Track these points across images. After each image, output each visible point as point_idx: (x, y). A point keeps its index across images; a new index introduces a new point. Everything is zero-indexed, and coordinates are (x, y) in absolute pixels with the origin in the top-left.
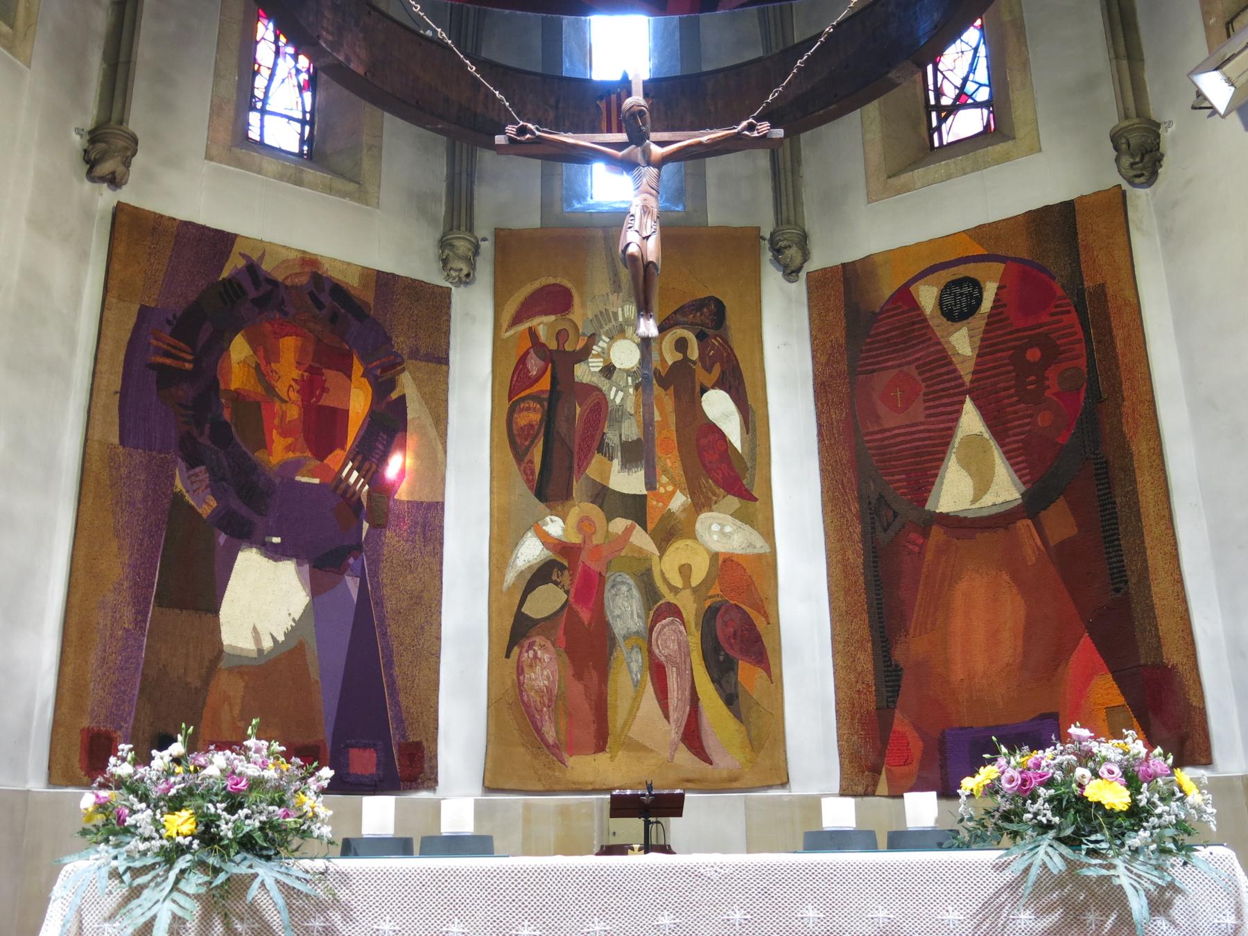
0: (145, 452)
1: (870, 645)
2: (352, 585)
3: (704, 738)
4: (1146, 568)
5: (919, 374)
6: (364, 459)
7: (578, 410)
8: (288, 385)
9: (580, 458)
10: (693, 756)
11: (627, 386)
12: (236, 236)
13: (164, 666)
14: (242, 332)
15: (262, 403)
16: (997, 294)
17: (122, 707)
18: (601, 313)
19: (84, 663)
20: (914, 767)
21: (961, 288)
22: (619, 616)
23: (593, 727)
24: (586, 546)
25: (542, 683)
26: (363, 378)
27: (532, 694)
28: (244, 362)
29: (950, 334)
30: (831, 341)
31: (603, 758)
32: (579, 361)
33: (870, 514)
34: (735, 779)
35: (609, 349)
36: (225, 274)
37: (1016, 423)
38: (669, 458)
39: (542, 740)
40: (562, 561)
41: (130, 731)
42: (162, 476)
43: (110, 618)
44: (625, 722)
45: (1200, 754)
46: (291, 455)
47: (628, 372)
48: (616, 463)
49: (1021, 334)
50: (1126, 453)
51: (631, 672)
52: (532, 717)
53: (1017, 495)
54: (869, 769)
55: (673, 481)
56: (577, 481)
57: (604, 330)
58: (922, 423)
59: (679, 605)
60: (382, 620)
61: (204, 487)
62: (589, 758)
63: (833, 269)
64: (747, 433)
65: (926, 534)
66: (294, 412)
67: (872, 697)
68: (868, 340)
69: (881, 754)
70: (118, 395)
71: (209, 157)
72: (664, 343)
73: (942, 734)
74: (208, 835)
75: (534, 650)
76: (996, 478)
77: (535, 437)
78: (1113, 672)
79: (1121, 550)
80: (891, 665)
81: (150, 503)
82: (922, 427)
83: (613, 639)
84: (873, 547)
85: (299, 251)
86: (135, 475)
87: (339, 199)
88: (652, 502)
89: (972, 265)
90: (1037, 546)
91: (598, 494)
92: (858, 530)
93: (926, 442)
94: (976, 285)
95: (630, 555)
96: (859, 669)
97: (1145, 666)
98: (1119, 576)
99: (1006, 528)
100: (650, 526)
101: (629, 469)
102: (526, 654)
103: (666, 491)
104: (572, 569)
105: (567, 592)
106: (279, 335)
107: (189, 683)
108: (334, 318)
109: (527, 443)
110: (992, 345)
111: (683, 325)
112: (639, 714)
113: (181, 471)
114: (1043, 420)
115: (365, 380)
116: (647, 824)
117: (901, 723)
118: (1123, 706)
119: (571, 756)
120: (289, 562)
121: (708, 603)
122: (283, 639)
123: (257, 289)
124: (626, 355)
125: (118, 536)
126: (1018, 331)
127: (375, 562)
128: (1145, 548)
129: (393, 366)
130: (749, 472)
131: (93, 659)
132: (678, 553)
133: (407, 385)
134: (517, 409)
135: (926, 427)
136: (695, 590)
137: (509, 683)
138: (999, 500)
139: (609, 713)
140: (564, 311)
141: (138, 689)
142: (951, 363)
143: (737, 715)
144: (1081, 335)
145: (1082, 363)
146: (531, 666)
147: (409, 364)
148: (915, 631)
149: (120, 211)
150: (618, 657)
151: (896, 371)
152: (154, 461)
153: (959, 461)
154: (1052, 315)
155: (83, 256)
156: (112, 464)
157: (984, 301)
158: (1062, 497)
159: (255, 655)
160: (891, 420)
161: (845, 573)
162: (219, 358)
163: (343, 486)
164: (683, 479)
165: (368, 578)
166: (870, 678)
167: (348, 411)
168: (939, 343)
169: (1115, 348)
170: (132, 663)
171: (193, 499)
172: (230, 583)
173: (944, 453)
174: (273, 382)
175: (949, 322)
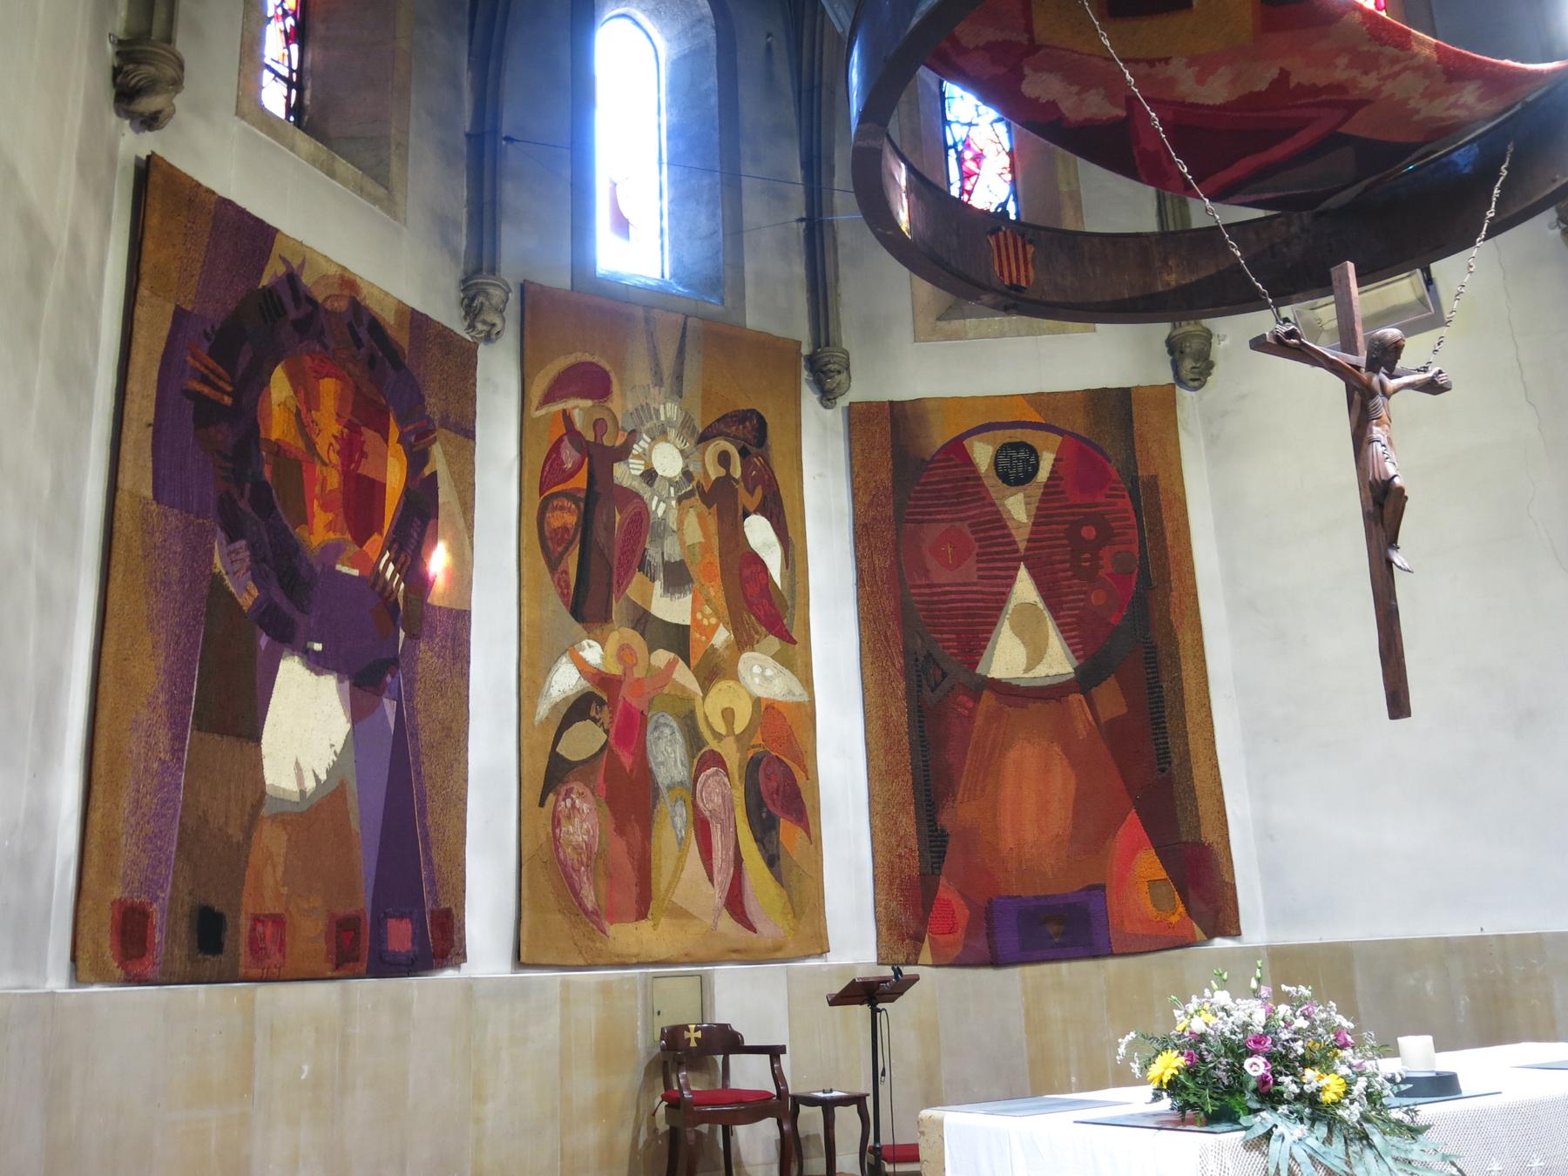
0: (181, 514)
1: (912, 807)
3: (746, 903)
4: (1188, 752)
5: (973, 533)
6: (401, 549)
7: (618, 518)
8: (328, 442)
9: (619, 574)
10: (736, 923)
11: (669, 497)
12: (277, 230)
13: (204, 812)
14: (283, 363)
15: (303, 463)
16: (1053, 466)
17: (158, 871)
18: (642, 407)
19: (114, 807)
20: (960, 934)
21: (1018, 453)
22: (662, 763)
23: (635, 890)
24: (627, 679)
25: (580, 838)
26: (398, 445)
27: (569, 850)
28: (283, 404)
29: (1005, 497)
30: (876, 482)
31: (645, 925)
32: (619, 459)
33: (917, 671)
35: (651, 450)
36: (265, 281)
37: (1071, 597)
38: (713, 586)
39: (580, 904)
40: (601, 695)
41: (167, 902)
42: (198, 554)
43: (143, 744)
44: (669, 884)
45: (1230, 926)
46: (332, 536)
47: (671, 482)
48: (658, 585)
49: (1076, 510)
50: (1172, 641)
51: (675, 827)
52: (569, 877)
53: (1070, 669)
54: (910, 937)
55: (716, 612)
56: (617, 602)
57: (645, 427)
58: (975, 584)
59: (722, 754)
60: (417, 754)
61: (245, 569)
62: (631, 926)
63: (880, 405)
64: (787, 568)
65: (976, 699)
66: (334, 480)
67: (916, 863)
68: (917, 488)
69: (923, 921)
70: (151, 428)
72: (707, 453)
73: (989, 903)
75: (572, 799)
76: (1049, 650)
77: (571, 543)
78: (1156, 848)
79: (1166, 733)
80: (937, 830)
81: (187, 586)
82: (975, 588)
83: (657, 789)
84: (919, 706)
85: (340, 266)
86: (171, 544)
87: (365, 202)
88: (695, 635)
89: (1029, 431)
90: (1088, 720)
91: (639, 620)
92: (903, 685)
93: (979, 604)
95: (673, 693)
96: (902, 833)
97: (1185, 843)
98: (1164, 755)
99: (1059, 701)
100: (694, 662)
101: (672, 594)
102: (563, 803)
103: (709, 623)
104: (612, 702)
105: (607, 732)
106: (322, 375)
107: (231, 836)
109: (560, 549)
110: (1046, 516)
111: (727, 436)
112: (684, 875)
113: (220, 544)
114: (1097, 599)
115: (400, 447)
116: (875, 1011)
117: (947, 891)
118: (1165, 880)
119: (612, 924)
120: (331, 677)
122: (325, 778)
123: (297, 308)
124: (668, 460)
125: (152, 629)
126: (1075, 506)
128: (1187, 733)
130: (789, 611)
131: (125, 804)
134: (550, 506)
135: (979, 588)
136: (738, 738)
137: (543, 837)
138: (1052, 672)
139: (653, 875)
140: (601, 397)
141: (175, 844)
142: (1005, 527)
143: (778, 877)
144: (1134, 521)
146: (569, 818)
147: (441, 433)
148: (963, 796)
150: (661, 811)
151: (949, 525)
152: (191, 528)
153: (1012, 628)
154: (1108, 496)
156: (145, 526)
157: (1040, 469)
158: (1113, 675)
159: (296, 798)
160: (942, 576)
161: (886, 730)
162: (259, 395)
163: (381, 582)
164: (726, 612)
165: (404, 702)
166: (913, 843)
167: (384, 486)
168: (993, 504)
169: (1165, 540)
170: (168, 809)
171: (233, 584)
172: (272, 701)
173: (997, 617)
174: (314, 436)
175: (1005, 485)
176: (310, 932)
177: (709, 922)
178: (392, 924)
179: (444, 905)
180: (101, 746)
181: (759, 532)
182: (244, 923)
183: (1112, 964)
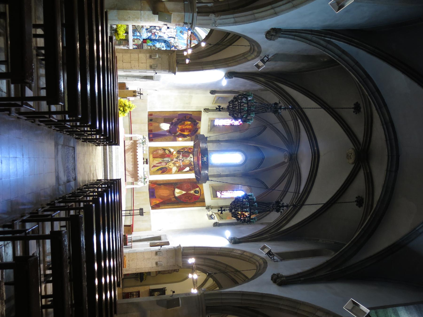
20: (152, 186)
23: (155, 157)
34: (150, 170)
36: (197, 121)
65: (173, 188)
66: (184, 128)
69: (153, 184)
71: (209, 118)
74: (144, 142)
83: (164, 159)
94: (198, 193)
98: (168, 204)
100: (175, 162)
104: (170, 154)
106: (191, 126)
108: (194, 131)
117: (155, 185)
127: (170, 136)
129: (190, 136)
132: (172, 165)
133: (188, 138)
136: (168, 166)
143: (156, 171)
145: (188, 202)
147: (191, 138)
149: (201, 111)
166: (160, 183)
167: (185, 132)
176: (151, 128)
177: (153, 164)
179: (153, 140)
180: (162, 112)
181: (187, 169)
182: (152, 123)
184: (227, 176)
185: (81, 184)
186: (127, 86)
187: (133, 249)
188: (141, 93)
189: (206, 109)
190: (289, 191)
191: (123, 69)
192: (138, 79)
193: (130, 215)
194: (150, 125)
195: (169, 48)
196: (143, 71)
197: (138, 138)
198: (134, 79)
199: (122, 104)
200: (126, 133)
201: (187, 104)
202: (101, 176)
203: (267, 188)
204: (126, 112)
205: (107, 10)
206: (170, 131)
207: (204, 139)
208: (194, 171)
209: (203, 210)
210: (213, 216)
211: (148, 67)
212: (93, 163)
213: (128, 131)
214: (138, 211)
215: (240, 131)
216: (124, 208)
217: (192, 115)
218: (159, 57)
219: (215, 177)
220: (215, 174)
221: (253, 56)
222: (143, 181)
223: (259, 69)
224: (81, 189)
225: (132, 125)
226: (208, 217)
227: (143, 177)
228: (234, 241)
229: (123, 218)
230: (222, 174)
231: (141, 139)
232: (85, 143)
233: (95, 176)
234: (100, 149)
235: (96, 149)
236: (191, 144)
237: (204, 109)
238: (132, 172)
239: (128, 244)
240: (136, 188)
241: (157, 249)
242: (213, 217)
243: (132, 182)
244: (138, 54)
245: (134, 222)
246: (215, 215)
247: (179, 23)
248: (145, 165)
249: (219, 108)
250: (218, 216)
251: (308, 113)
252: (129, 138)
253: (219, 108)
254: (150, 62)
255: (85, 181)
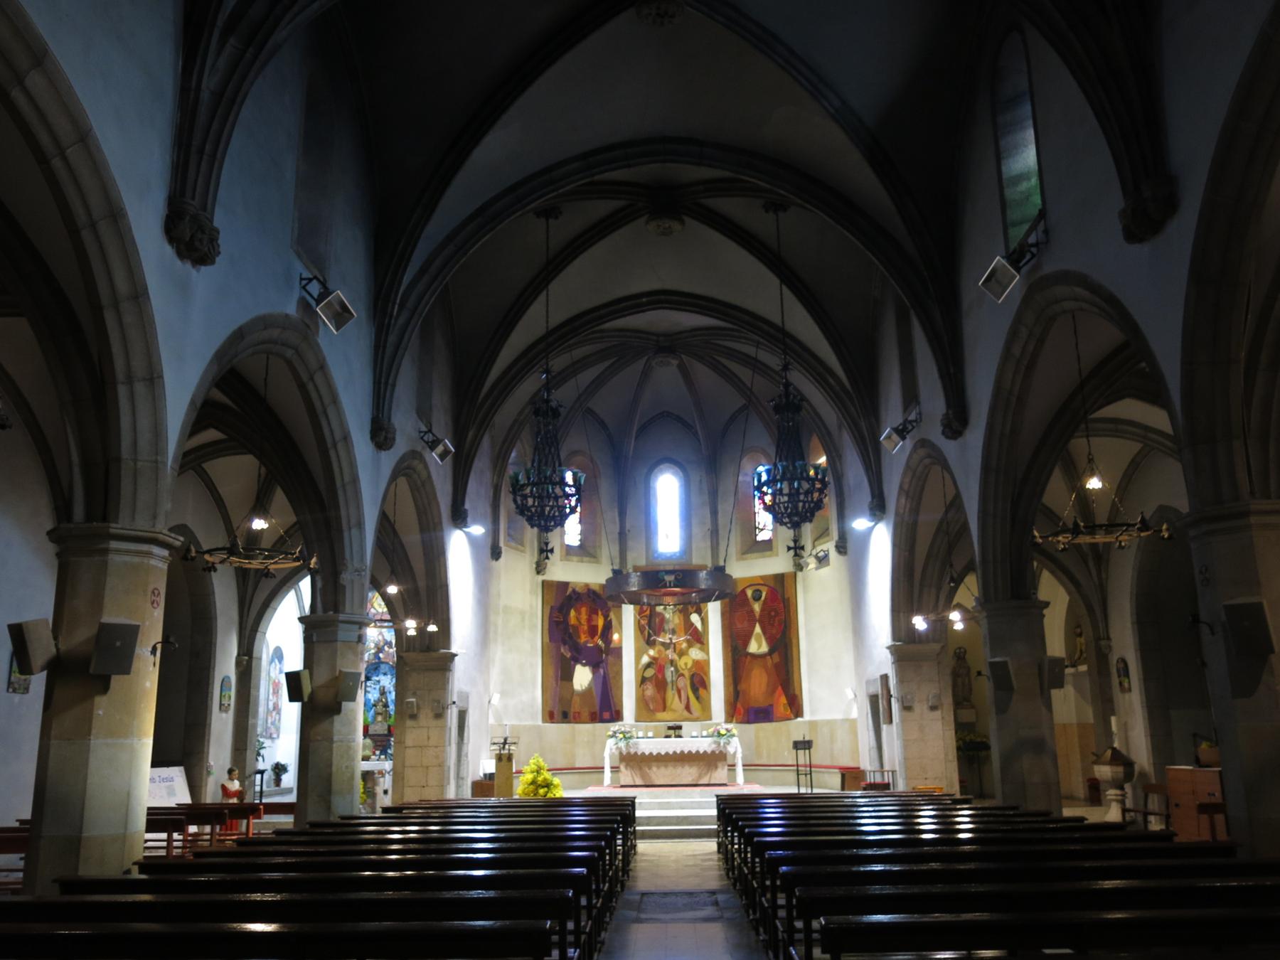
2: (601, 671)
36: (568, 593)
42: (559, 649)
50: (791, 640)
65: (746, 657)
66: (586, 628)
71: (561, 560)
74: (624, 737)
94: (761, 592)
100: (677, 652)
104: (657, 663)
108: (594, 600)
117: (739, 705)
121: (691, 673)
127: (607, 664)
132: (684, 659)
133: (612, 616)
145: (783, 617)
147: (612, 609)
149: (544, 582)
155: (537, 595)
160: (739, 626)
176: (585, 714)
178: (604, 713)
179: (617, 709)
181: (695, 618)
182: (572, 714)
183: (774, 724)
184: (714, 513)
185: (726, 882)
186: (480, 777)
187: (897, 769)
188: (502, 741)
189: (536, 568)
190: (754, 356)
191: (443, 786)
192: (465, 748)
193: (811, 774)
194: (577, 719)
195: (379, 666)
196: (448, 735)
197: (614, 751)
198: (463, 758)
199: (531, 790)
200: (600, 783)
201: (523, 620)
202: (711, 845)
203: (745, 407)
204: (549, 782)
205: (307, 823)
206: (595, 665)
207: (619, 576)
208: (702, 605)
209: (804, 580)
210: (819, 555)
211: (439, 722)
212: (676, 861)
213: (595, 776)
214: (801, 752)
215: (595, 477)
216: (793, 790)
217: (551, 607)
218: (414, 694)
219: (718, 544)
220: (709, 543)
221: (420, 467)
222: (725, 741)
223: (452, 451)
224: (736, 880)
225: (577, 766)
226: (822, 568)
227: (715, 739)
228: (878, 509)
229: (815, 791)
230: (709, 525)
231: (617, 744)
232: (631, 873)
233: (710, 857)
234: (642, 846)
235: (643, 855)
236: (629, 613)
237: (538, 573)
238: (702, 768)
239: (886, 781)
240: (743, 759)
241: (897, 705)
242: (821, 554)
243: (726, 768)
244: (406, 747)
245: (835, 764)
246: (819, 549)
247: (150, 593)
248: (683, 732)
249: (547, 551)
250: (821, 541)
251: (557, 318)
252: (615, 775)
253: (547, 551)
254: (425, 718)
255: (721, 875)
